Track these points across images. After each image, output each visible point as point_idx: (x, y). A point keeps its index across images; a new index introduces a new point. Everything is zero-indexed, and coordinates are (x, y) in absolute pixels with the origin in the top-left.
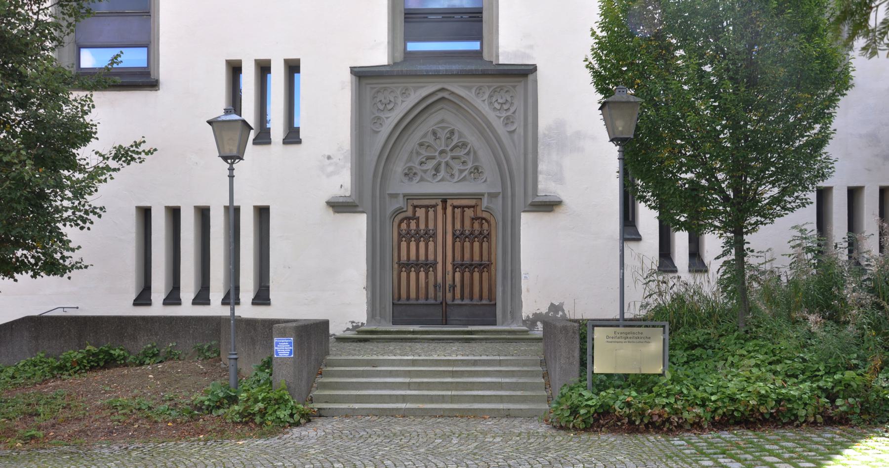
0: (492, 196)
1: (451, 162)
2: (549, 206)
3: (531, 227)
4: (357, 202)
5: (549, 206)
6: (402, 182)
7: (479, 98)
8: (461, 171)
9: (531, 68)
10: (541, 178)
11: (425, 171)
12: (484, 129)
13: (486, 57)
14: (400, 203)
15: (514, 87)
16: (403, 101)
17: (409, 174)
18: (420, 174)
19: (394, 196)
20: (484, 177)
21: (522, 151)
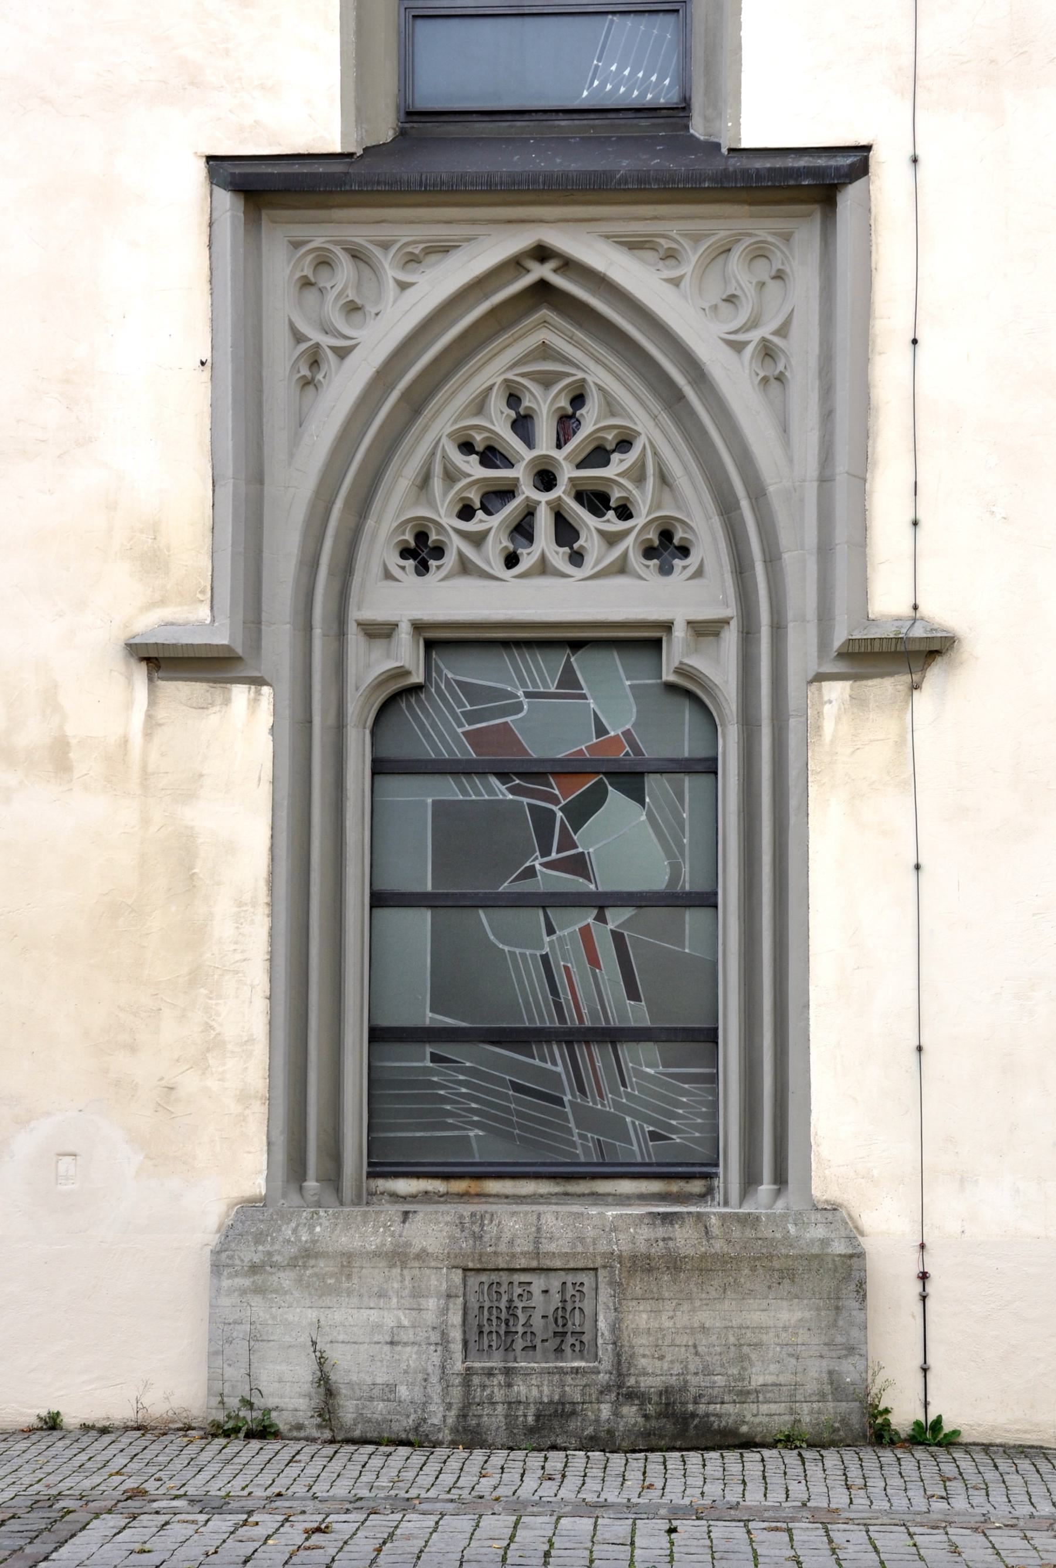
0: (705, 630)
1: (511, 509)
2: (914, 654)
3: (844, 735)
4: (239, 651)
5: (914, 654)
6: (388, 576)
7: (669, 281)
8: (611, 539)
9: (845, 161)
10: (264, 614)
11: (477, 540)
12: (674, 382)
13: (698, 129)
14: (406, 654)
15: (787, 238)
16: (403, 286)
17: (421, 551)
18: (456, 544)
19: (380, 632)
20: (693, 561)
21: (812, 469)
